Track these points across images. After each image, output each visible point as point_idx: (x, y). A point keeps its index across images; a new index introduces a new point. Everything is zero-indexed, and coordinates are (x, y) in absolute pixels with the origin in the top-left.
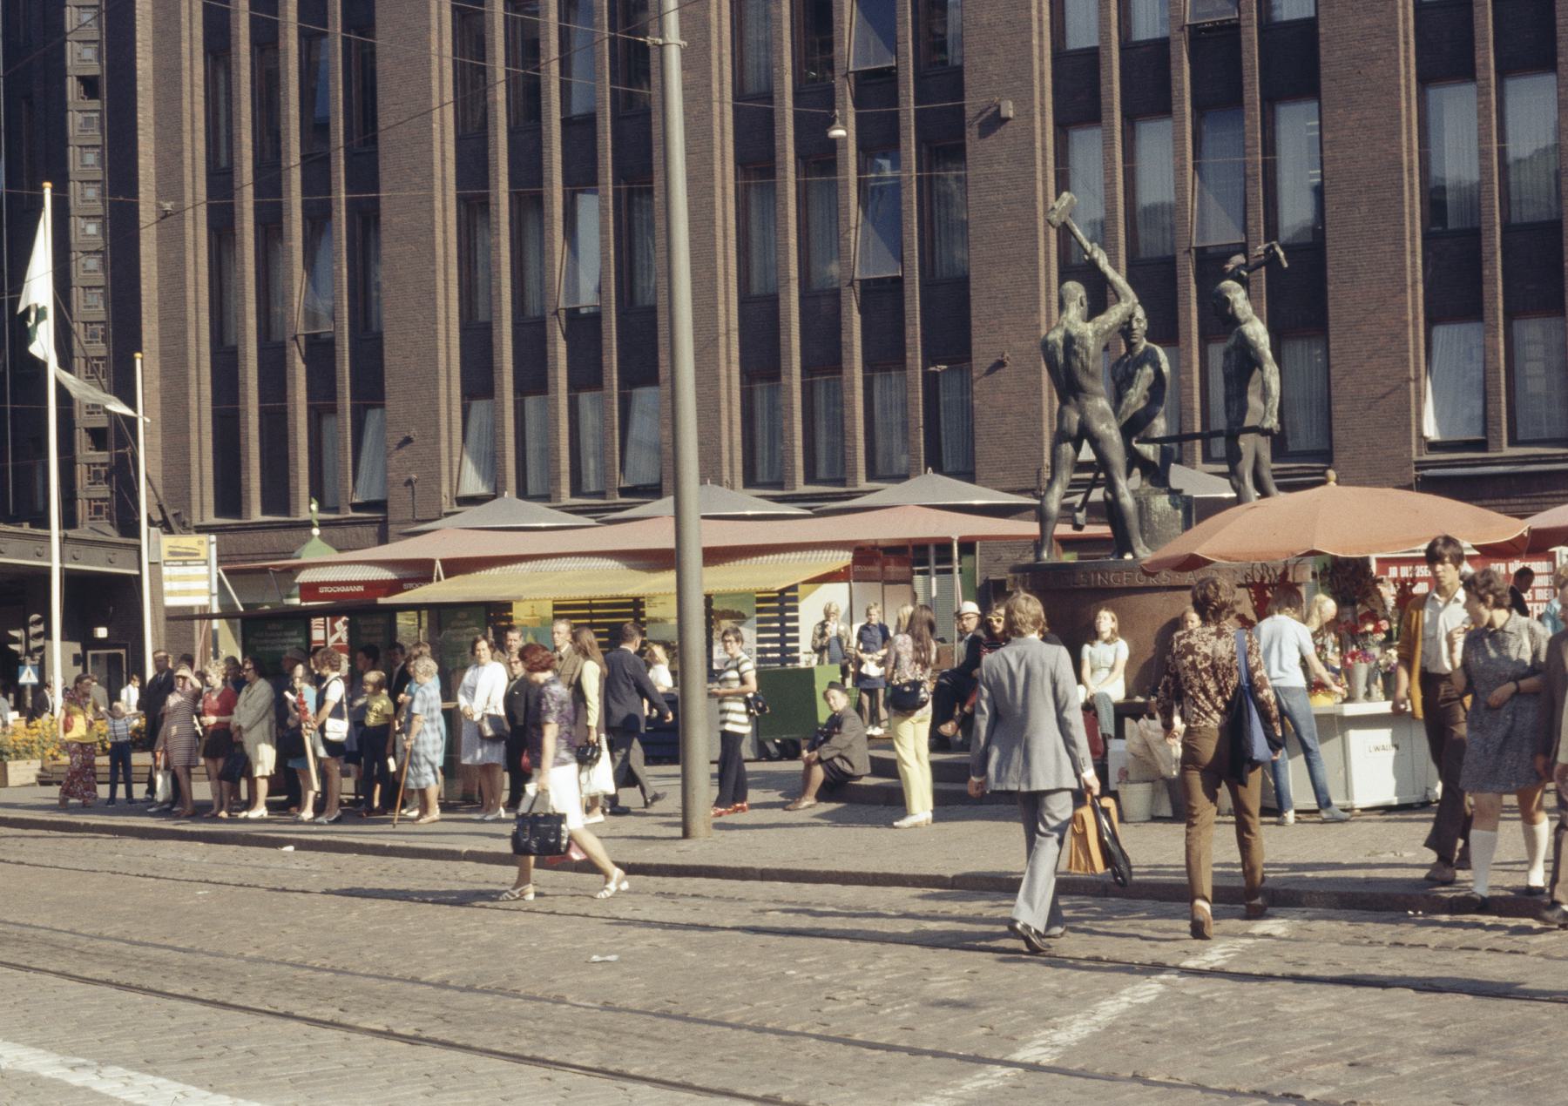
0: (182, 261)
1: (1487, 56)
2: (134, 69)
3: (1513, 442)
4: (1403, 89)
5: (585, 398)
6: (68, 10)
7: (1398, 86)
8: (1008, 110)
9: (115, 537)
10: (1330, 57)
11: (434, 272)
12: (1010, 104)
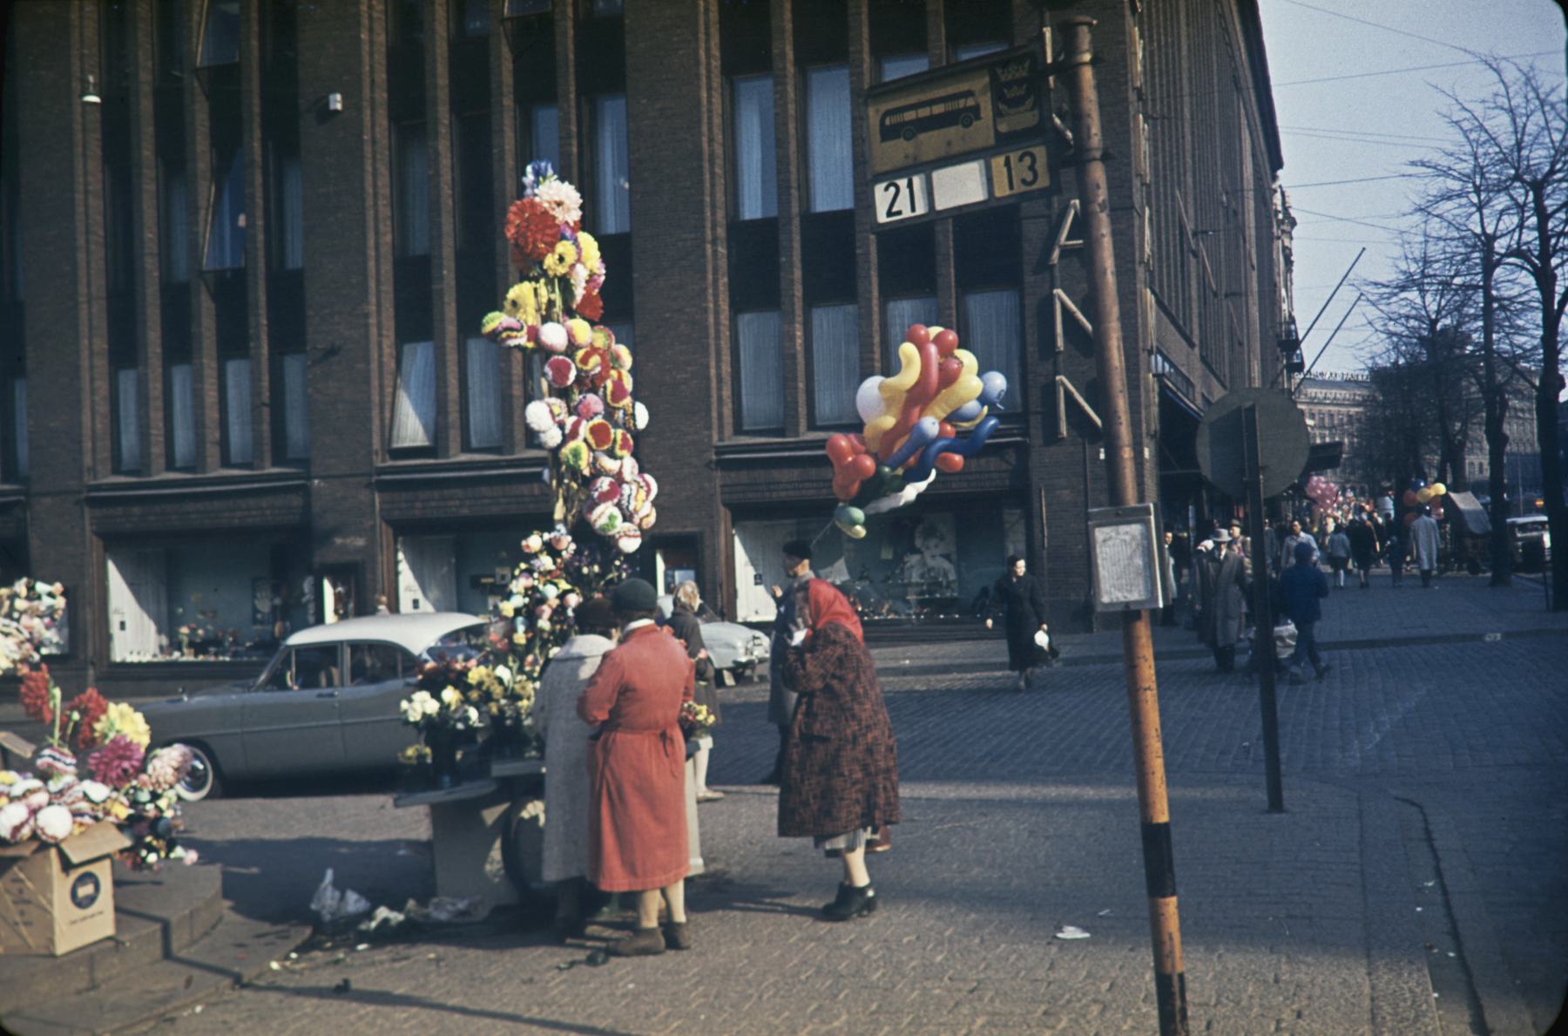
4: (704, 80)
5: (232, 367)
7: (698, 76)
12: (338, 97)
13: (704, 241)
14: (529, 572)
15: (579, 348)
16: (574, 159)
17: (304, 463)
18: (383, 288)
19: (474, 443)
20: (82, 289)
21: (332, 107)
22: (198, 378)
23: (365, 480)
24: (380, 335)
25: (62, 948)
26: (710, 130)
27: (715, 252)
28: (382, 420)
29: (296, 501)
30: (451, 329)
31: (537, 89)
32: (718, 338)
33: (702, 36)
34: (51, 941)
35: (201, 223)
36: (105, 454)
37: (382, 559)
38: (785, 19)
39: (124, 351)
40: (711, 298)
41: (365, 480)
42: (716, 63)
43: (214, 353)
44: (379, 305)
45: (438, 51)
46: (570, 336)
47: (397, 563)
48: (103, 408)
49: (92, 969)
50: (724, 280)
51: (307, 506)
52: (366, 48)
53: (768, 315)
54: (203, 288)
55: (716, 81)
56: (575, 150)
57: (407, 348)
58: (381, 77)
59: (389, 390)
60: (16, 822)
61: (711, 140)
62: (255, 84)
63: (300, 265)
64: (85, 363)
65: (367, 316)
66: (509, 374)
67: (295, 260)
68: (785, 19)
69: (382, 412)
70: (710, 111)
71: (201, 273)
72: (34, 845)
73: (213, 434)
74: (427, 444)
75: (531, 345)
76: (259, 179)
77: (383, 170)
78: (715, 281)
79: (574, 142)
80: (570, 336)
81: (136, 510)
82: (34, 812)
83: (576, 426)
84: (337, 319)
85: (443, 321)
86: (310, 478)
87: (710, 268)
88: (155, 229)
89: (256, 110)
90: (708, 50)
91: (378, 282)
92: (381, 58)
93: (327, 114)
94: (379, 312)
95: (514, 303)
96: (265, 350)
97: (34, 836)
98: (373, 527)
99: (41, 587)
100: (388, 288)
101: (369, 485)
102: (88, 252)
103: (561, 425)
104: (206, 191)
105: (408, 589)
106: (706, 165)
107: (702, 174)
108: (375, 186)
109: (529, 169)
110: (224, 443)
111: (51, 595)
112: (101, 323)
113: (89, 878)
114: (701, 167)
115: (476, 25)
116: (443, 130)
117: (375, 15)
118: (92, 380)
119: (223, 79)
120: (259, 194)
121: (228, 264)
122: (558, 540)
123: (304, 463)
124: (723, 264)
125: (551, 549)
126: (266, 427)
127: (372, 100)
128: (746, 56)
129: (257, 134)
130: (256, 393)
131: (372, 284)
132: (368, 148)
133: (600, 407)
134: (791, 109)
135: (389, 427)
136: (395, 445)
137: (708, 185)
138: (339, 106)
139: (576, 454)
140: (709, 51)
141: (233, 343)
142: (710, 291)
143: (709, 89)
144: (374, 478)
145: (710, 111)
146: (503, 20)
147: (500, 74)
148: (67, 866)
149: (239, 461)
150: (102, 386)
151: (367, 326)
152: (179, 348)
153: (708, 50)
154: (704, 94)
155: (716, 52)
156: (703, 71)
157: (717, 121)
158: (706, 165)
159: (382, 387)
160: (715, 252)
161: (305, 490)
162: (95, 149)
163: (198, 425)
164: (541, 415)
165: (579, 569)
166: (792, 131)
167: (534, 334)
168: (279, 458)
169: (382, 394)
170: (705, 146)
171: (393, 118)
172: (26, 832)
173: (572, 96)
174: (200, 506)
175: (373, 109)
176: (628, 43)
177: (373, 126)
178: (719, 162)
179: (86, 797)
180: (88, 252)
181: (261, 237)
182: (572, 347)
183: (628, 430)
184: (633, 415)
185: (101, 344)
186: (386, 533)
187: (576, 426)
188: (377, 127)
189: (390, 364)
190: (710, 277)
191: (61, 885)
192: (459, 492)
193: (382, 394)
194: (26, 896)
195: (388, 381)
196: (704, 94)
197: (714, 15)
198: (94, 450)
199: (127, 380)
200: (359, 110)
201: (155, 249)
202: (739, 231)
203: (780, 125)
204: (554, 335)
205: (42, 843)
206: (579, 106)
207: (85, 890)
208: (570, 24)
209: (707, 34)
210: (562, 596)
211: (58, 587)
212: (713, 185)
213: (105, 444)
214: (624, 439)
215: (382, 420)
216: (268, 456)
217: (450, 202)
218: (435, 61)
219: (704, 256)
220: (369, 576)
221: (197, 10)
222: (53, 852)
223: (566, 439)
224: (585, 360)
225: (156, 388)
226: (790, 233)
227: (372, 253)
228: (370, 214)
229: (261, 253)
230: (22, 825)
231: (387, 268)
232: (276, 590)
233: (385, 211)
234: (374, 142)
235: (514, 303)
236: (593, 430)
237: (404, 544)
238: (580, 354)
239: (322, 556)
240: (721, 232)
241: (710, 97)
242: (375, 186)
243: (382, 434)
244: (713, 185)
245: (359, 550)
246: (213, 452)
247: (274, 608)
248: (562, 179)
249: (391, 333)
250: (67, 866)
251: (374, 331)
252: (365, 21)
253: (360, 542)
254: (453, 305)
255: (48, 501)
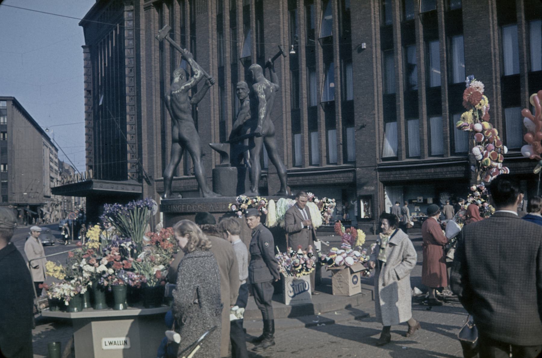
0: (152, 107)
1: (522, 15)
2: (381, 35)
3: (430, 155)
4: (492, 28)
5: (330, 132)
6: (125, 31)
7: (490, 27)
8: (364, 46)
9: (137, 183)
10: (467, 19)
11: (210, 107)
12: (365, 44)
13: (493, 84)
14: (473, 196)
15: (485, 130)
16: (445, 59)
17: (354, 162)
18: (379, 105)
19: (410, 156)
20: (284, 110)
21: (363, 48)
22: (320, 136)
23: (374, 168)
24: (379, 120)
25: (350, 295)
26: (494, 45)
27: (496, 87)
28: (379, 148)
29: (351, 175)
30: (402, 118)
31: (431, 35)
32: (498, 117)
33: (491, 13)
34: (348, 292)
35: (321, 87)
36: (291, 161)
37: (380, 194)
38: (521, 5)
39: (296, 128)
40: (495, 103)
41: (374, 168)
42: (496, 22)
43: (324, 128)
44: (378, 111)
45: (397, 26)
46: (483, 126)
47: (384, 195)
48: (290, 146)
49: (358, 301)
50: (500, 97)
51: (355, 177)
52: (373, 27)
53: (517, 108)
54: (321, 108)
55: (496, 28)
56: (445, 56)
57: (387, 124)
58: (378, 36)
59: (381, 138)
60: (340, 260)
61: (494, 49)
62: (338, 43)
63: (351, 99)
64: (285, 132)
65: (374, 114)
66: (423, 132)
67: (350, 97)
68: (521, 5)
69: (379, 145)
70: (494, 39)
71: (321, 103)
72: (345, 267)
73: (324, 154)
74: (394, 156)
75: (471, 130)
76: (339, 72)
77: (379, 67)
78: (497, 97)
79: (445, 53)
80: (483, 126)
81: (301, 178)
82: (344, 258)
83: (487, 153)
84: (364, 116)
85: (400, 115)
86: (355, 168)
87: (495, 93)
88: (306, 90)
89: (338, 50)
90: (493, 18)
91: (378, 103)
92: (378, 30)
93: (360, 50)
94: (378, 113)
95: (464, 118)
96: (341, 127)
97: (344, 264)
98: (377, 183)
99: (329, 200)
100: (381, 105)
101: (375, 170)
102: (286, 98)
103: (482, 154)
104: (322, 76)
105: (388, 204)
106: (493, 57)
107: (491, 60)
108: (377, 72)
109: (467, 78)
110: (327, 157)
111: (332, 202)
112: (289, 120)
113: (355, 276)
114: (491, 58)
115: (409, 16)
116: (399, 52)
117: (376, 16)
118: (287, 138)
119: (328, 41)
120: (339, 77)
121: (328, 100)
122: (482, 187)
123: (354, 162)
124: (499, 91)
125: (479, 189)
126: (341, 151)
127: (376, 44)
128: (507, 17)
129: (338, 58)
130: (338, 140)
131: (376, 104)
132: (374, 60)
133: (493, 148)
134: (524, 35)
135: (381, 151)
136: (384, 156)
137: (493, 64)
138: (365, 47)
139: (487, 161)
140: (493, 18)
141: (331, 124)
142: (495, 101)
143: (494, 31)
144: (377, 168)
145: (494, 39)
146: (419, 14)
147: (419, 32)
148: (352, 272)
149: (332, 162)
150: (290, 139)
151: (374, 118)
152: (314, 126)
153: (493, 18)
154: (492, 33)
155: (496, 18)
156: (491, 25)
157: (497, 42)
158: (493, 57)
159: (379, 137)
160: (496, 87)
161: (354, 171)
162: (288, 66)
163: (320, 151)
164: (477, 150)
165: (486, 195)
166: (524, 43)
167: (473, 127)
168: (345, 161)
169: (379, 140)
170: (492, 51)
171: (383, 49)
172: (343, 263)
173: (444, 37)
174: (321, 177)
175: (376, 47)
176: (464, 18)
177: (376, 53)
178: (497, 56)
179: (355, 255)
180: (286, 98)
181: (339, 91)
182: (484, 130)
183: (502, 154)
184: (503, 150)
185: (290, 126)
186: (381, 185)
187: (487, 153)
188: (377, 52)
189: (382, 129)
190: (495, 96)
191: (350, 277)
192: (405, 172)
193: (379, 140)
194: (341, 280)
195: (381, 136)
196: (492, 33)
197: (495, 5)
198: (287, 160)
199: (297, 137)
200: (371, 47)
201: (306, 96)
202: (505, 80)
203: (520, 41)
204: (478, 127)
205: (346, 266)
206: (446, 40)
207: (355, 280)
208: (443, 13)
209: (492, 12)
210: (483, 203)
211: (334, 200)
212: (495, 64)
213: (291, 157)
214: (501, 157)
215: (379, 148)
216: (342, 161)
217: (402, 75)
218: (396, 30)
219: (492, 89)
220: (375, 199)
221: (319, 20)
222: (348, 269)
223: (483, 158)
224: (487, 134)
225: (306, 139)
226: (524, 79)
227: (376, 94)
228: (375, 81)
229: (340, 96)
230: (342, 261)
231: (381, 99)
232: (344, 204)
233: (380, 80)
234: (376, 57)
235: (464, 118)
236: (492, 155)
237: (387, 189)
238: (486, 132)
239: (360, 192)
240: (499, 80)
241: (494, 33)
242: (377, 72)
243: (380, 153)
244: (495, 64)
245: (373, 191)
246: (324, 160)
247: (343, 209)
248: (478, 80)
249: (382, 120)
250: (352, 272)
251: (377, 119)
252: (373, 19)
253: (373, 188)
254: (403, 110)
255: (272, 175)
